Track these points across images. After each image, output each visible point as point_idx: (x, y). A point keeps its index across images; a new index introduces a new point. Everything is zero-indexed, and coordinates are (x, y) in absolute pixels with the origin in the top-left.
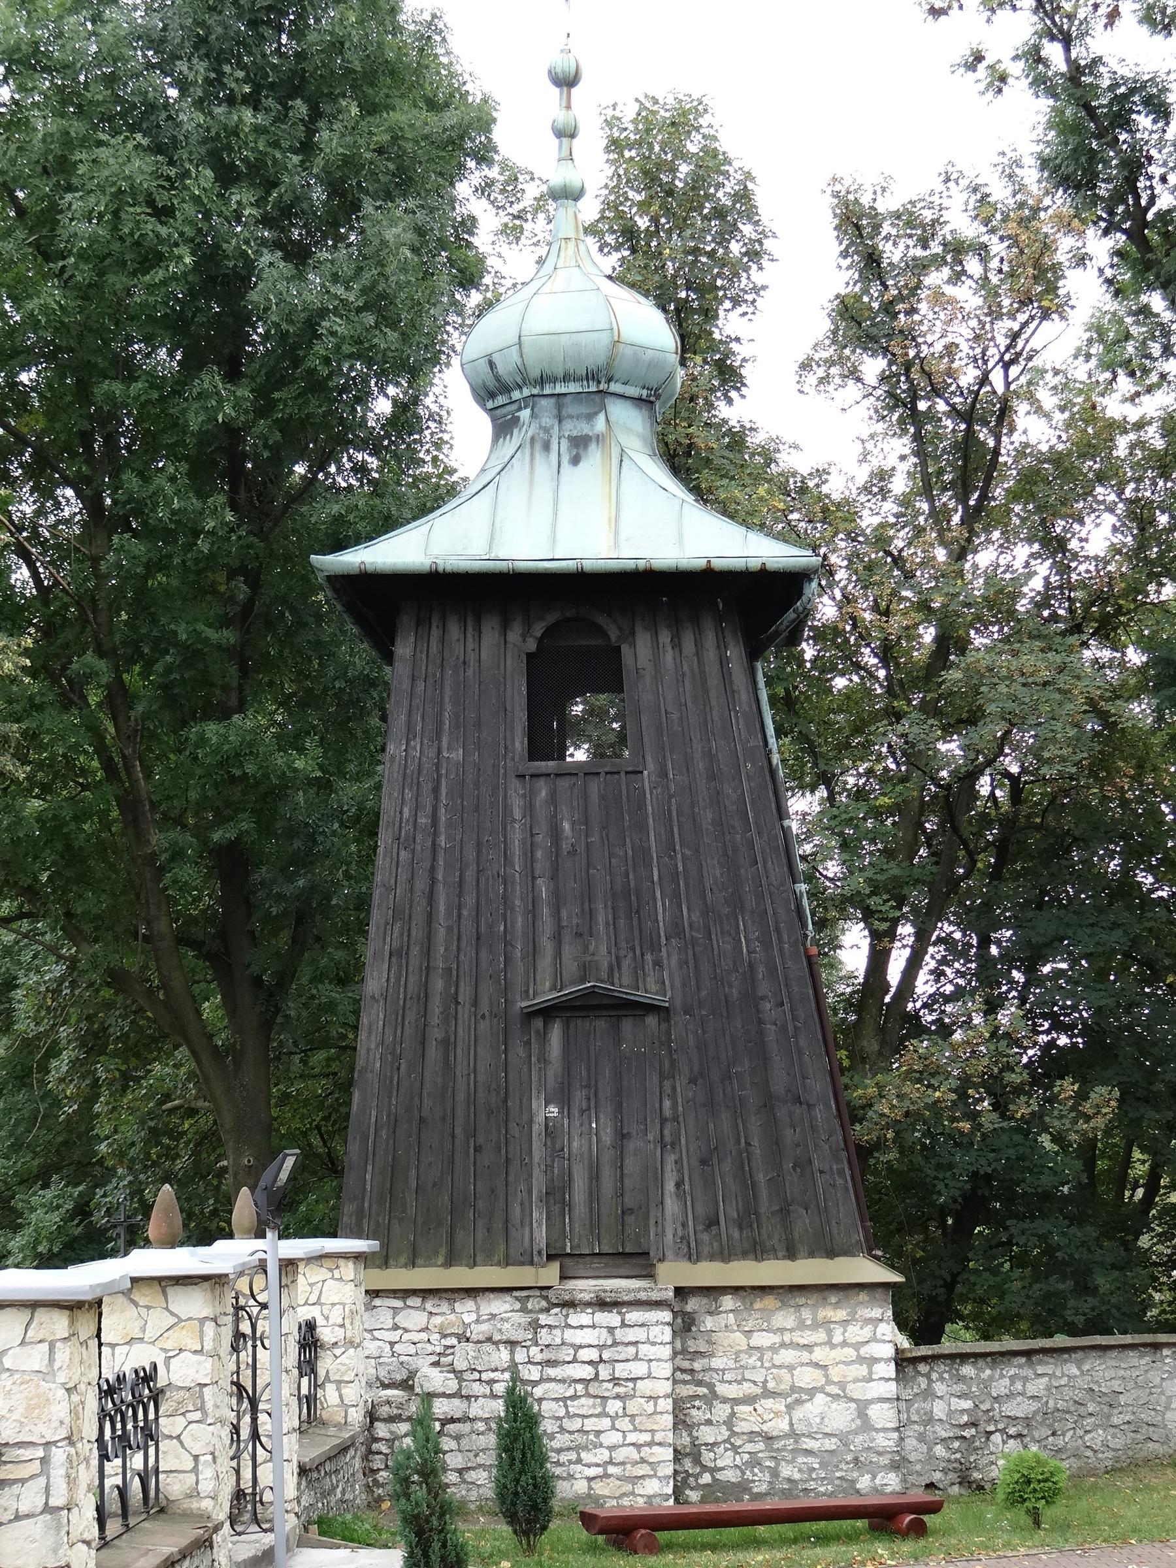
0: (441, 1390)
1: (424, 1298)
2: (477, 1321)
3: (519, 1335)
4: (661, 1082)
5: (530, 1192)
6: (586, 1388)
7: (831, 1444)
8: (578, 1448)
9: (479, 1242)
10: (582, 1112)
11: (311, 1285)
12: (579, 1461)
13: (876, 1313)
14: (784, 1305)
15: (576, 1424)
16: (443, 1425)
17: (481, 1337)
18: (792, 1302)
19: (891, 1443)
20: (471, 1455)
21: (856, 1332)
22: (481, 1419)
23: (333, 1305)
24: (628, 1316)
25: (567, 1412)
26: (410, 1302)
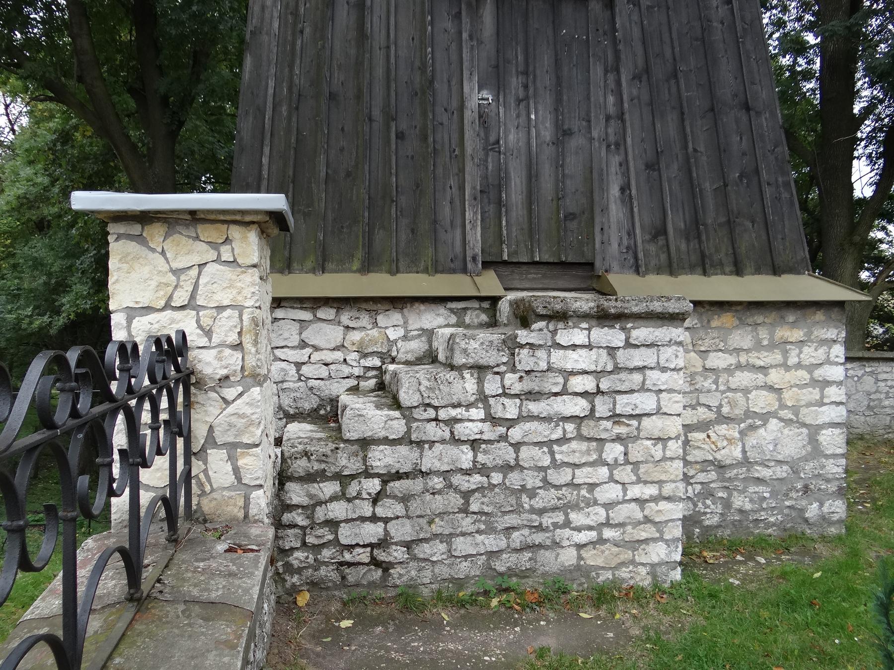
0: (382, 434)
1: (338, 309)
2: (405, 338)
3: (492, 358)
4: (605, 75)
5: (462, 188)
6: (578, 429)
7: (782, 472)
8: (566, 508)
9: (402, 245)
10: (519, 101)
11: (177, 272)
12: (567, 524)
13: (831, 333)
14: (742, 323)
15: (563, 476)
16: (385, 483)
17: (410, 357)
18: (750, 321)
19: (840, 470)
20: (423, 522)
21: (810, 354)
22: (438, 473)
23: (220, 308)
24: (635, 333)
25: (554, 460)
26: (321, 314)
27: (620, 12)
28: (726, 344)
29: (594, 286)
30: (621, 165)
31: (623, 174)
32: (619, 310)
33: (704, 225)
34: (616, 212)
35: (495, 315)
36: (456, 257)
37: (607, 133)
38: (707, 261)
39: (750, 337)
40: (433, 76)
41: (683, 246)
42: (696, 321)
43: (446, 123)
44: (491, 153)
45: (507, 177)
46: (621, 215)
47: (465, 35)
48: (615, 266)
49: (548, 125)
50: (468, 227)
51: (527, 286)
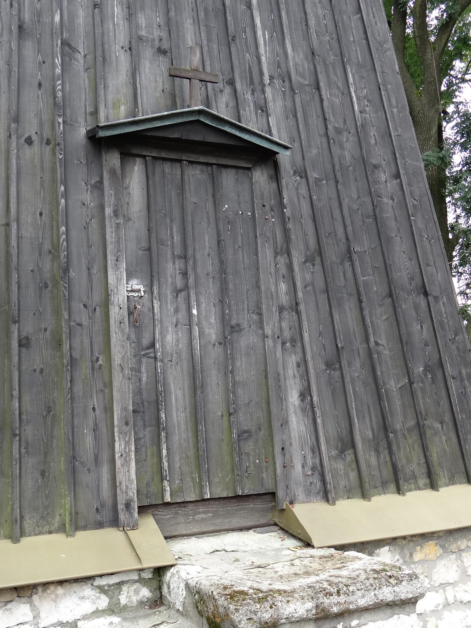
4: (275, 257)
5: (109, 410)
10: (177, 292)
18: (453, 547)
27: (287, 185)
28: (431, 580)
29: (276, 520)
30: (298, 366)
31: (302, 377)
32: (343, 607)
33: (394, 432)
34: (297, 425)
35: (160, 588)
36: (103, 506)
37: (281, 329)
38: (401, 475)
39: (455, 567)
40: (68, 262)
41: (373, 460)
42: (398, 557)
43: (85, 323)
44: (144, 360)
45: (166, 390)
46: (303, 428)
47: (108, 211)
48: (300, 493)
49: (212, 321)
50: (118, 463)
51: (195, 530)
